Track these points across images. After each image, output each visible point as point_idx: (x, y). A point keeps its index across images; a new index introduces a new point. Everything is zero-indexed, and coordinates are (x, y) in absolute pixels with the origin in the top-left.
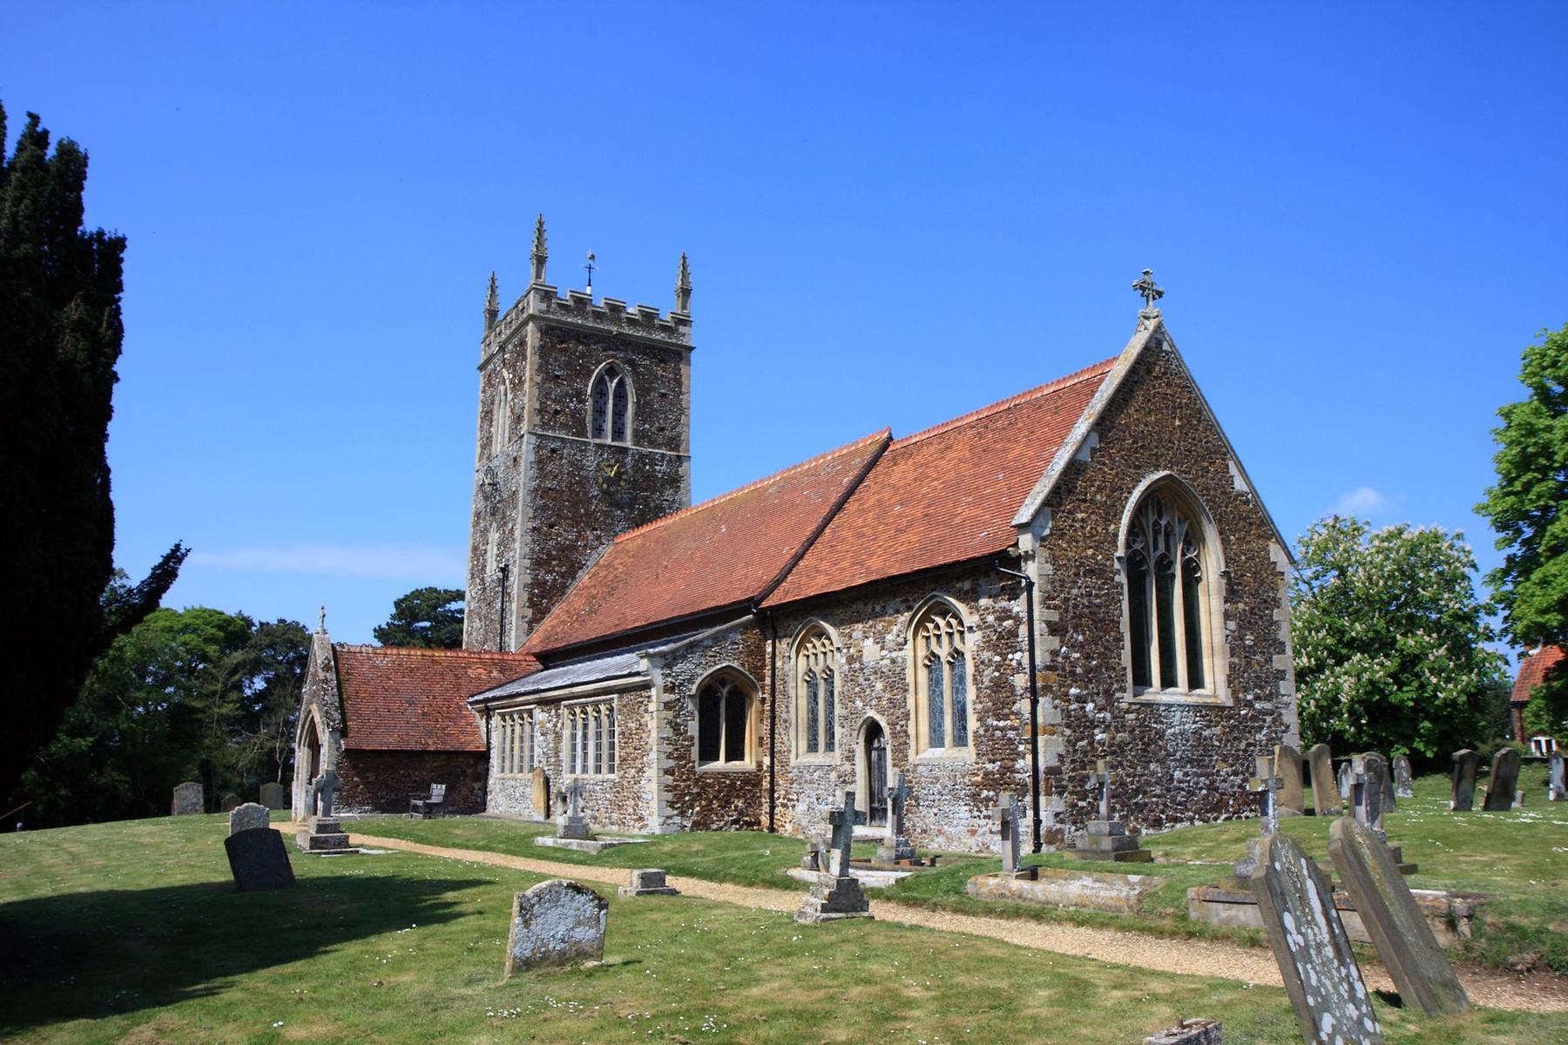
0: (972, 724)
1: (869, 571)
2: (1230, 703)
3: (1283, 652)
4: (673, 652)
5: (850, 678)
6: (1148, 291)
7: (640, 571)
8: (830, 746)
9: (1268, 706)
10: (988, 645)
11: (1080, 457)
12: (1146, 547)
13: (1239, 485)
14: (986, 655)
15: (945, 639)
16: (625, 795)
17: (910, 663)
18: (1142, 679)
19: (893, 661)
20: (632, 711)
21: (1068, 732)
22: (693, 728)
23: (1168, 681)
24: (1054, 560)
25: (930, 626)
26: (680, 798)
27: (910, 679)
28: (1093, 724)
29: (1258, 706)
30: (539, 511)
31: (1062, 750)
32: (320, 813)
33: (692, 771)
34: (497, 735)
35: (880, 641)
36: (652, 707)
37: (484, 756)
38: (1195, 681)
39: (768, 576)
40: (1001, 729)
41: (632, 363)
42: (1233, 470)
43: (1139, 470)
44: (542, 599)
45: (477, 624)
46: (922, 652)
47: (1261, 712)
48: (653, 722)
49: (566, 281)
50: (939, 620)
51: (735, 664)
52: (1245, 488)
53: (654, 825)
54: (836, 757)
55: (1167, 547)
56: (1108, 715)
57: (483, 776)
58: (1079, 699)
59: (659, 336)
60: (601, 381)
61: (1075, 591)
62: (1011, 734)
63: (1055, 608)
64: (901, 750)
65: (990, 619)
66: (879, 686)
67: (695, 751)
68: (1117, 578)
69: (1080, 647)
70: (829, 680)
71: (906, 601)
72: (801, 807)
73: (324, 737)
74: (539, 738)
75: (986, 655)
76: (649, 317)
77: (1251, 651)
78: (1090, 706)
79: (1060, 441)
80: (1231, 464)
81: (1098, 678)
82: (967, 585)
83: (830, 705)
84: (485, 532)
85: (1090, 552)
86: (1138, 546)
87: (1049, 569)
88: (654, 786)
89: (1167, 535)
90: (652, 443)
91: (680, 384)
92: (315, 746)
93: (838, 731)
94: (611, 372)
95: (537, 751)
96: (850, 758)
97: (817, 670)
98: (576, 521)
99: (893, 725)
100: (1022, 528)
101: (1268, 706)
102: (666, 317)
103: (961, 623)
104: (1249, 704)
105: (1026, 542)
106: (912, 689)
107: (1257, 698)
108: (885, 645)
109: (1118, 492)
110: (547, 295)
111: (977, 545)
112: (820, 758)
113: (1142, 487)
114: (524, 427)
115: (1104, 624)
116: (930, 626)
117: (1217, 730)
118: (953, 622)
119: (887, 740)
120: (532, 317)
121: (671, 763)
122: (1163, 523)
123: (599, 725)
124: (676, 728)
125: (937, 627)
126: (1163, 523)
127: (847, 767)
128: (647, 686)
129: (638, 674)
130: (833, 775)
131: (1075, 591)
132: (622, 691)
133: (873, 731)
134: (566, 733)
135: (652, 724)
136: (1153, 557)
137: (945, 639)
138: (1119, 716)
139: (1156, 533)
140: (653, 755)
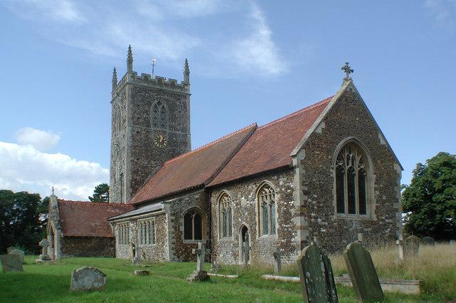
0: (277, 226)
1: (243, 173)
2: (376, 220)
3: (398, 202)
4: (173, 202)
5: (237, 211)
6: (348, 70)
7: (170, 177)
8: (230, 235)
9: (391, 221)
10: (282, 198)
11: (317, 131)
12: (344, 164)
13: (382, 142)
14: (282, 202)
15: (268, 197)
16: (159, 250)
17: (257, 205)
18: (341, 210)
19: (251, 205)
20: (160, 222)
21: (310, 229)
22: (182, 228)
23: (352, 211)
24: (305, 168)
25: (264, 192)
26: (177, 252)
27: (257, 211)
28: (321, 226)
29: (387, 221)
30: (133, 154)
31: (308, 235)
32: (371, 208)
33: (182, 243)
34: (116, 232)
35: (247, 198)
36: (167, 221)
37: (113, 239)
38: (363, 211)
39: (209, 176)
40: (287, 228)
41: (167, 101)
42: (380, 136)
43: (341, 136)
44: (135, 186)
45: (114, 194)
46: (221, 208)
47: (388, 223)
48: (167, 227)
49: (140, 69)
50: (266, 190)
51: (198, 207)
52: (384, 143)
53: (168, 258)
54: (233, 238)
55: (353, 164)
56: (327, 223)
57: (114, 246)
58: (315, 218)
59: (179, 90)
60: (156, 106)
61: (314, 180)
62: (290, 229)
63: (306, 185)
64: (254, 235)
65: (283, 189)
66: (246, 214)
67: (183, 236)
68: (331, 175)
69: (316, 199)
70: (230, 212)
71: (255, 184)
72: (221, 255)
73: (56, 232)
74: (131, 232)
75: (282, 202)
76: (173, 83)
77: (384, 202)
78: (319, 220)
79: (309, 127)
80: (380, 135)
81: (323, 210)
82: (276, 177)
83: (230, 220)
84: (115, 162)
85: (320, 166)
86: (341, 164)
87: (304, 171)
88: (167, 248)
89: (353, 160)
90: (176, 130)
91: (186, 108)
92: (53, 235)
93: (233, 229)
94: (159, 103)
95: (131, 237)
96: (237, 239)
97: (226, 208)
98: (147, 157)
99: (251, 227)
100: (294, 156)
101: (391, 221)
102: (179, 82)
103: (274, 191)
104: (383, 220)
105: (295, 162)
106: (257, 215)
107: (386, 218)
108: (246, 199)
109: (335, 143)
110: (134, 75)
111: (280, 163)
112: (226, 239)
113: (342, 143)
114: (126, 123)
115: (325, 191)
116: (264, 192)
117: (370, 229)
118: (272, 191)
119: (249, 233)
120: (128, 83)
121: (175, 240)
122: (351, 155)
123: (150, 227)
124: (175, 228)
125: (266, 193)
126: (351, 155)
127: (236, 242)
128: (164, 214)
129: (161, 210)
130: (232, 245)
131: (314, 180)
132: (157, 216)
133: (245, 229)
134: (139, 230)
135: (167, 227)
136: (347, 168)
137: (268, 197)
138: (331, 224)
139: (348, 159)
140: (167, 238)
